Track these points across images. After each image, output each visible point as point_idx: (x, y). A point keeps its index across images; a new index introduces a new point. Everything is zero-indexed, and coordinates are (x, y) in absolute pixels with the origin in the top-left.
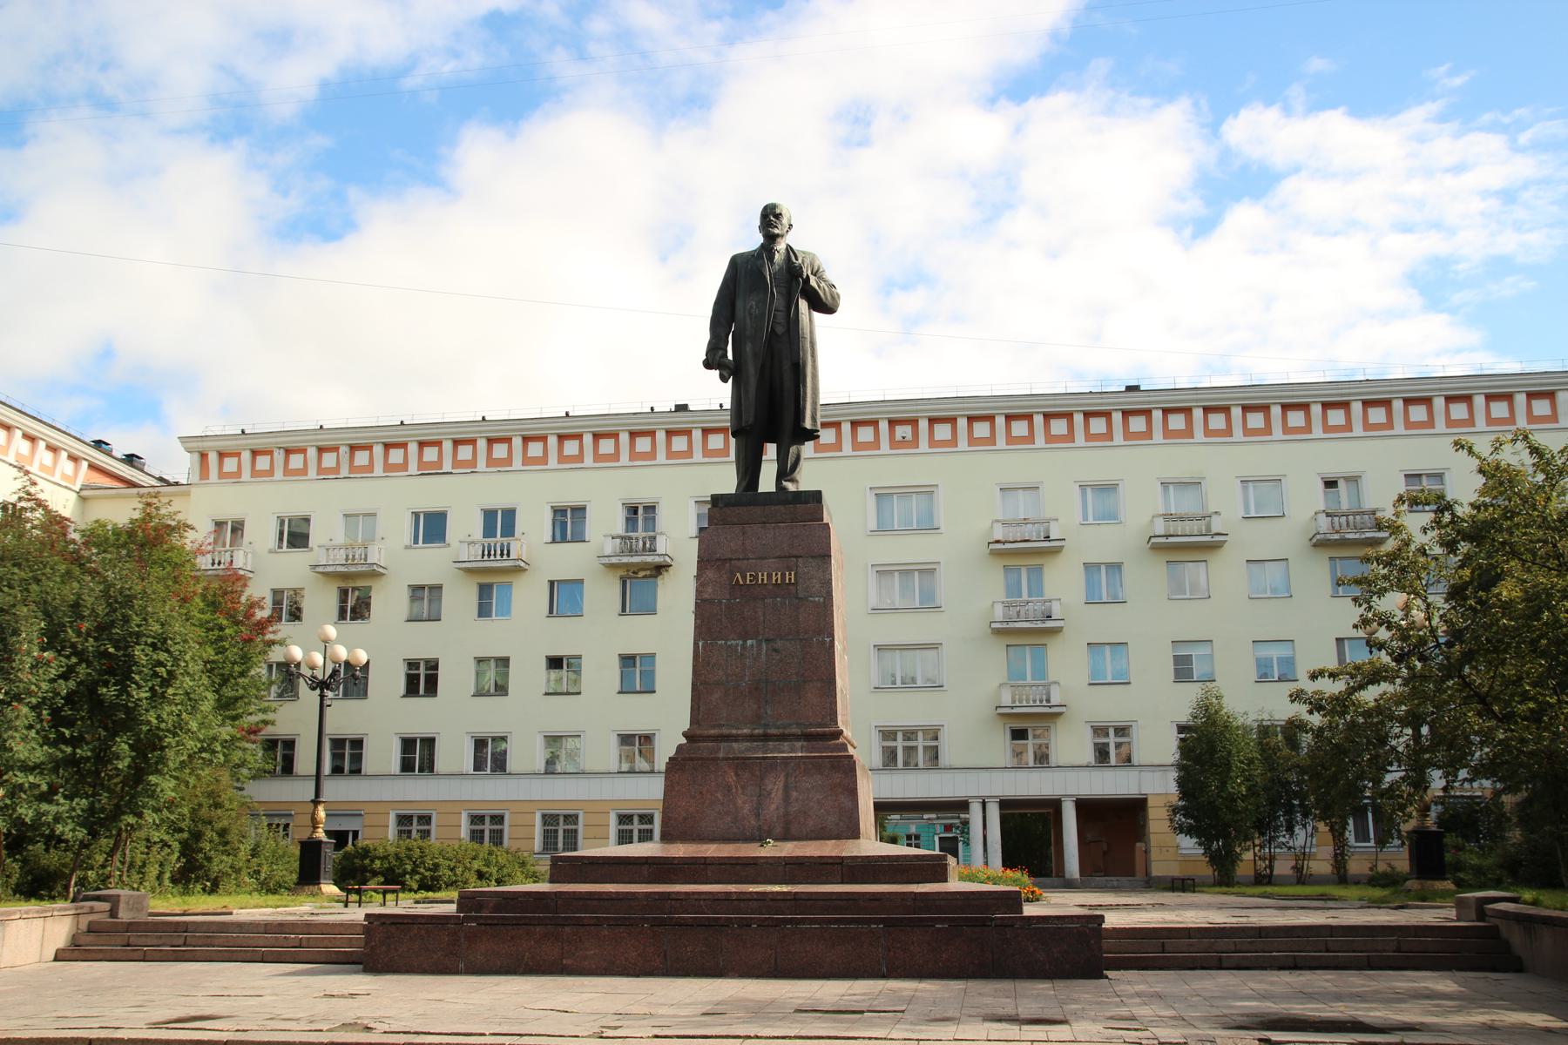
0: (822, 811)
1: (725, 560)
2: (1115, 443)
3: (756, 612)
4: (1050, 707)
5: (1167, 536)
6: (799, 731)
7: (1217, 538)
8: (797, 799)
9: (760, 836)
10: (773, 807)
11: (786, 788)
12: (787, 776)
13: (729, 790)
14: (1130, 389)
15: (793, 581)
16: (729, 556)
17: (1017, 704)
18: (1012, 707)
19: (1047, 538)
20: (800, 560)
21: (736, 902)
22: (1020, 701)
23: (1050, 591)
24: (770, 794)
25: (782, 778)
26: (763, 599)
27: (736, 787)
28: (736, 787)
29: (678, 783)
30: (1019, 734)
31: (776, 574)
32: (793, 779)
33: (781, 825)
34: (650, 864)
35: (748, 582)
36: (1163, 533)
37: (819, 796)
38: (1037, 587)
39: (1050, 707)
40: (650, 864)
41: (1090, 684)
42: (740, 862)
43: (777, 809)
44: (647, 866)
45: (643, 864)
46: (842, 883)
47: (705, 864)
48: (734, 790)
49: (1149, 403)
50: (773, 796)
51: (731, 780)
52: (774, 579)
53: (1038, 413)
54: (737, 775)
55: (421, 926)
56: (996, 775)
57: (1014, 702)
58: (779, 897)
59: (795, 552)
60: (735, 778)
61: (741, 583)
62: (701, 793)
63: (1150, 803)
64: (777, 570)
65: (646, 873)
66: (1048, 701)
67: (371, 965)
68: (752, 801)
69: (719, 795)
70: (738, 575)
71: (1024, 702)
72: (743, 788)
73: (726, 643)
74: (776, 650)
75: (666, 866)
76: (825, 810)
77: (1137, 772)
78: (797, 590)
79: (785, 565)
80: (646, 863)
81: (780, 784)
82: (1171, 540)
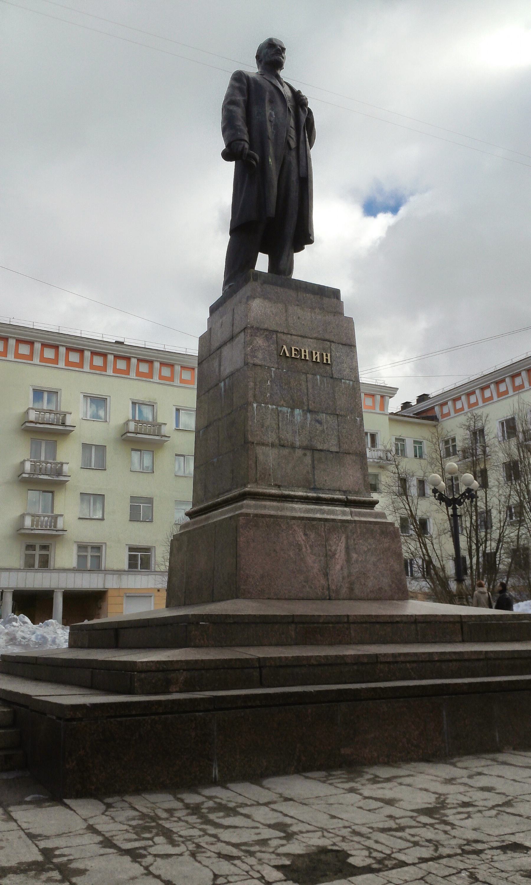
0: (378, 573)
1: (258, 329)
2: (108, 373)
3: (300, 385)
4: (57, 531)
5: (519, 393)
6: (344, 497)
7: (164, 438)
8: (357, 561)
9: (330, 596)
10: (338, 567)
11: (347, 548)
12: (347, 538)
13: (300, 550)
14: (117, 342)
15: (329, 362)
16: (276, 329)
17: (35, 527)
18: (32, 530)
19: (63, 424)
20: (333, 344)
21: (438, 664)
22: (37, 526)
23: (61, 457)
24: (335, 554)
25: (343, 539)
26: (306, 374)
27: (306, 548)
28: (306, 548)
29: (253, 541)
30: (30, 547)
31: (316, 353)
32: (352, 541)
33: (346, 585)
34: (296, 623)
35: (293, 356)
36: (133, 431)
37: (373, 559)
38: (53, 453)
39: (57, 531)
40: (296, 623)
41: (80, 518)
42: (378, 620)
43: (342, 569)
44: (293, 626)
45: (289, 623)
46: (463, 641)
47: (348, 622)
48: (304, 550)
49: (130, 353)
50: (337, 556)
51: (300, 539)
52: (314, 357)
53: (63, 346)
54: (305, 535)
55: (157, 718)
56: (13, 574)
57: (32, 526)
58: (473, 657)
59: (327, 337)
60: (304, 538)
61: (288, 355)
62: (275, 550)
63: (110, 594)
64: (315, 348)
65: (293, 633)
66: (55, 526)
67: (93, 787)
68: (320, 561)
69: (291, 553)
70: (285, 347)
71: (48, 527)
72: (311, 547)
73: (277, 408)
74: (320, 422)
75: (311, 626)
76: (380, 572)
77: (104, 575)
78: (332, 371)
79: (321, 347)
80: (293, 622)
81: (342, 546)
82: (139, 436)
